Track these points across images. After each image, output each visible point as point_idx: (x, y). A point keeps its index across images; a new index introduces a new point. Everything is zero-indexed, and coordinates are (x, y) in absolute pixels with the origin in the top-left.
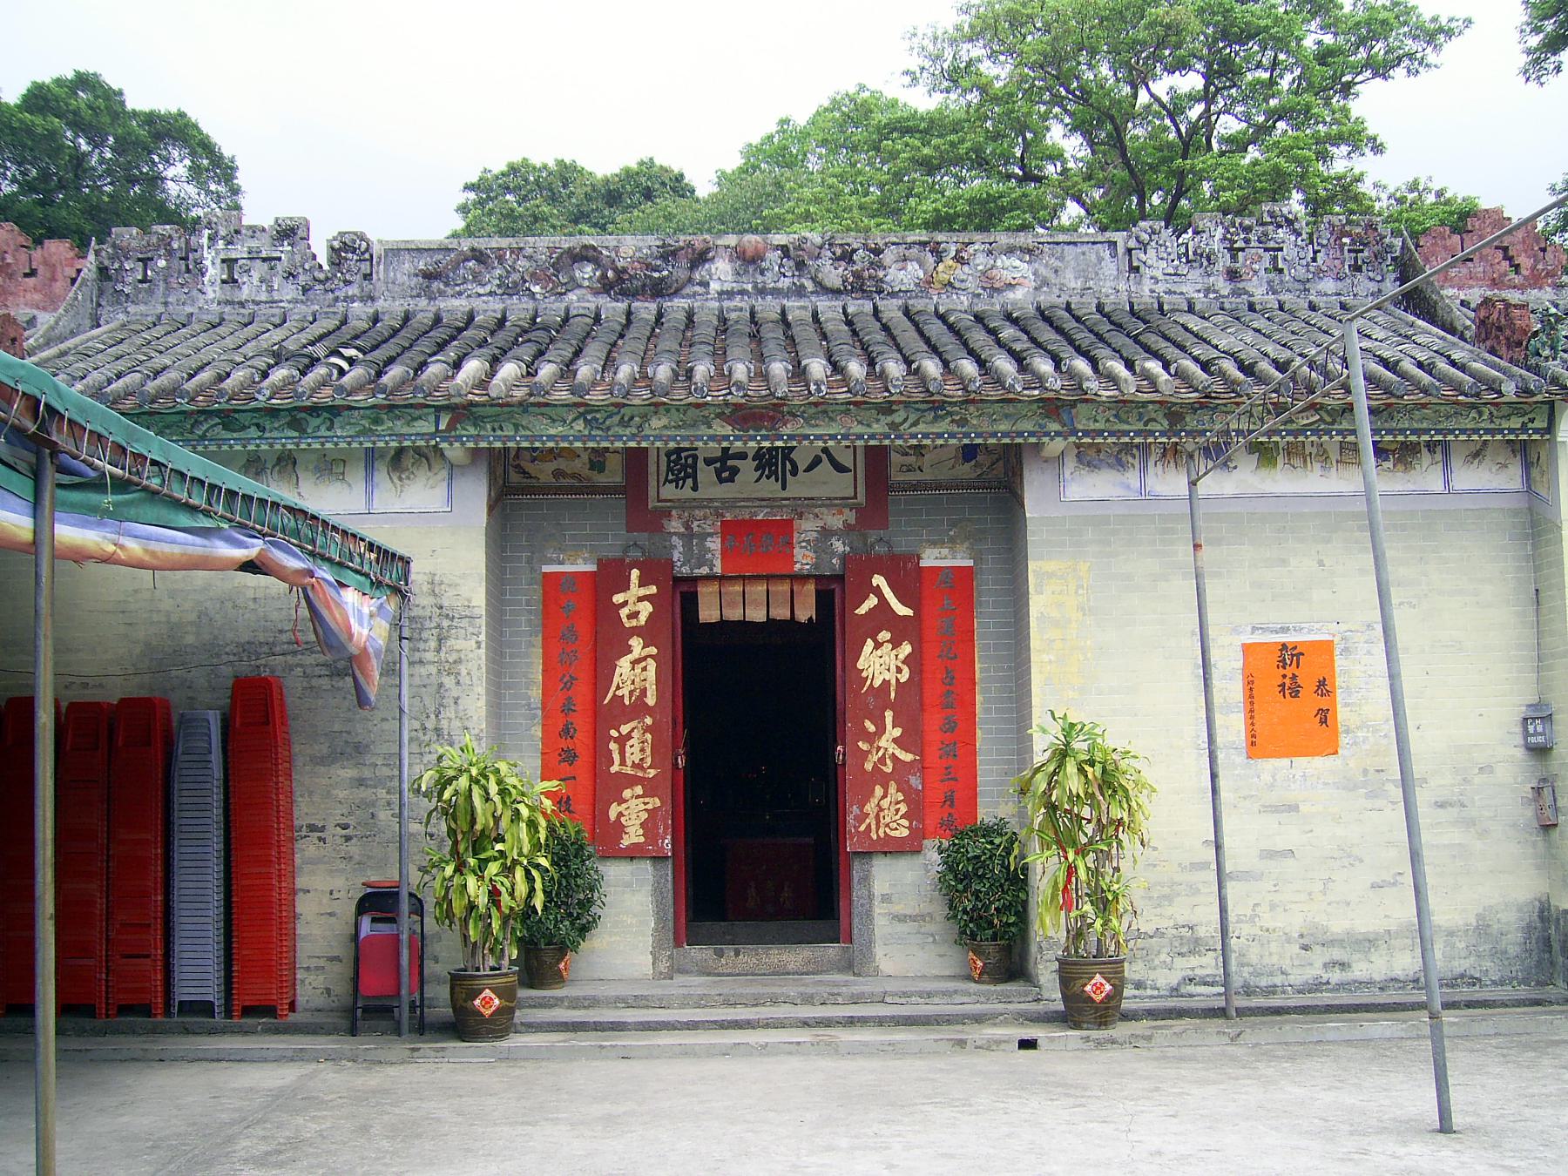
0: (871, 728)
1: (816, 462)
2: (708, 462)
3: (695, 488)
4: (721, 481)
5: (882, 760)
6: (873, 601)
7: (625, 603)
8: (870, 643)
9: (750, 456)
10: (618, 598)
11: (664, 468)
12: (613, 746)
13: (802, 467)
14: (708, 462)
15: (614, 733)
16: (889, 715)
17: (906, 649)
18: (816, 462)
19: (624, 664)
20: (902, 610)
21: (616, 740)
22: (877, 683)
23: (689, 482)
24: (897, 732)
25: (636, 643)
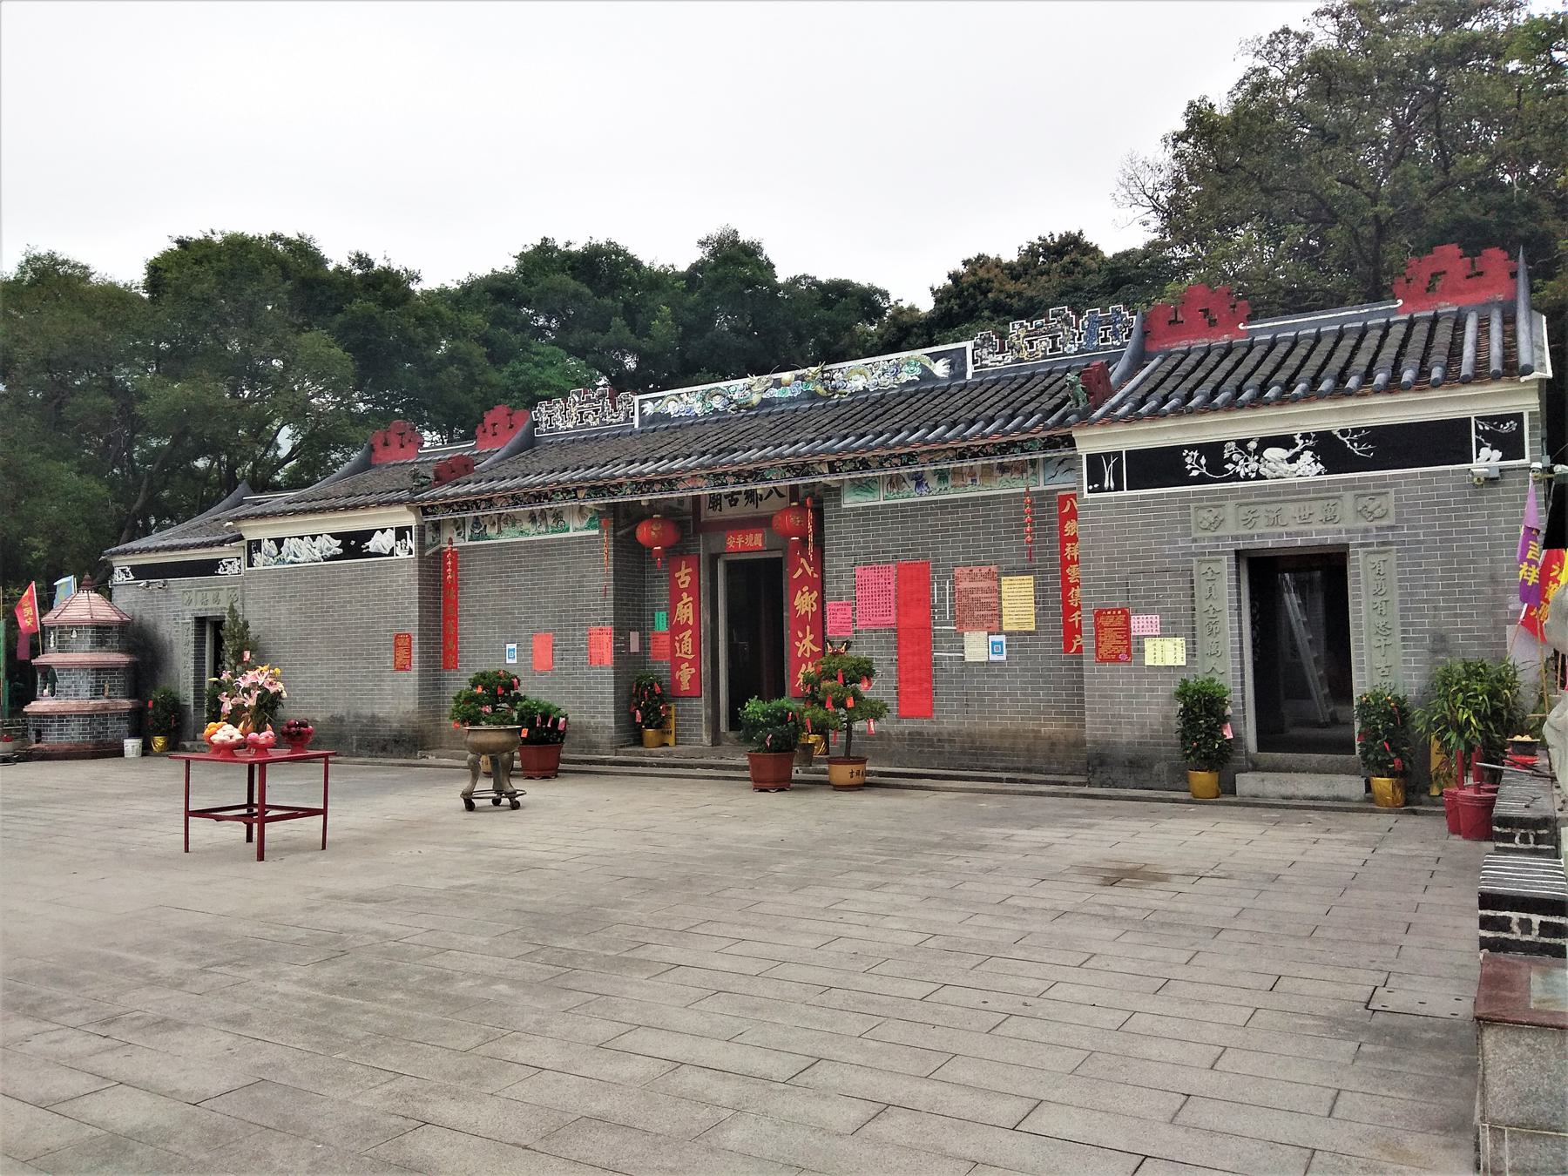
6: (800, 571)
17: (815, 594)
19: (680, 605)
25: (685, 595)
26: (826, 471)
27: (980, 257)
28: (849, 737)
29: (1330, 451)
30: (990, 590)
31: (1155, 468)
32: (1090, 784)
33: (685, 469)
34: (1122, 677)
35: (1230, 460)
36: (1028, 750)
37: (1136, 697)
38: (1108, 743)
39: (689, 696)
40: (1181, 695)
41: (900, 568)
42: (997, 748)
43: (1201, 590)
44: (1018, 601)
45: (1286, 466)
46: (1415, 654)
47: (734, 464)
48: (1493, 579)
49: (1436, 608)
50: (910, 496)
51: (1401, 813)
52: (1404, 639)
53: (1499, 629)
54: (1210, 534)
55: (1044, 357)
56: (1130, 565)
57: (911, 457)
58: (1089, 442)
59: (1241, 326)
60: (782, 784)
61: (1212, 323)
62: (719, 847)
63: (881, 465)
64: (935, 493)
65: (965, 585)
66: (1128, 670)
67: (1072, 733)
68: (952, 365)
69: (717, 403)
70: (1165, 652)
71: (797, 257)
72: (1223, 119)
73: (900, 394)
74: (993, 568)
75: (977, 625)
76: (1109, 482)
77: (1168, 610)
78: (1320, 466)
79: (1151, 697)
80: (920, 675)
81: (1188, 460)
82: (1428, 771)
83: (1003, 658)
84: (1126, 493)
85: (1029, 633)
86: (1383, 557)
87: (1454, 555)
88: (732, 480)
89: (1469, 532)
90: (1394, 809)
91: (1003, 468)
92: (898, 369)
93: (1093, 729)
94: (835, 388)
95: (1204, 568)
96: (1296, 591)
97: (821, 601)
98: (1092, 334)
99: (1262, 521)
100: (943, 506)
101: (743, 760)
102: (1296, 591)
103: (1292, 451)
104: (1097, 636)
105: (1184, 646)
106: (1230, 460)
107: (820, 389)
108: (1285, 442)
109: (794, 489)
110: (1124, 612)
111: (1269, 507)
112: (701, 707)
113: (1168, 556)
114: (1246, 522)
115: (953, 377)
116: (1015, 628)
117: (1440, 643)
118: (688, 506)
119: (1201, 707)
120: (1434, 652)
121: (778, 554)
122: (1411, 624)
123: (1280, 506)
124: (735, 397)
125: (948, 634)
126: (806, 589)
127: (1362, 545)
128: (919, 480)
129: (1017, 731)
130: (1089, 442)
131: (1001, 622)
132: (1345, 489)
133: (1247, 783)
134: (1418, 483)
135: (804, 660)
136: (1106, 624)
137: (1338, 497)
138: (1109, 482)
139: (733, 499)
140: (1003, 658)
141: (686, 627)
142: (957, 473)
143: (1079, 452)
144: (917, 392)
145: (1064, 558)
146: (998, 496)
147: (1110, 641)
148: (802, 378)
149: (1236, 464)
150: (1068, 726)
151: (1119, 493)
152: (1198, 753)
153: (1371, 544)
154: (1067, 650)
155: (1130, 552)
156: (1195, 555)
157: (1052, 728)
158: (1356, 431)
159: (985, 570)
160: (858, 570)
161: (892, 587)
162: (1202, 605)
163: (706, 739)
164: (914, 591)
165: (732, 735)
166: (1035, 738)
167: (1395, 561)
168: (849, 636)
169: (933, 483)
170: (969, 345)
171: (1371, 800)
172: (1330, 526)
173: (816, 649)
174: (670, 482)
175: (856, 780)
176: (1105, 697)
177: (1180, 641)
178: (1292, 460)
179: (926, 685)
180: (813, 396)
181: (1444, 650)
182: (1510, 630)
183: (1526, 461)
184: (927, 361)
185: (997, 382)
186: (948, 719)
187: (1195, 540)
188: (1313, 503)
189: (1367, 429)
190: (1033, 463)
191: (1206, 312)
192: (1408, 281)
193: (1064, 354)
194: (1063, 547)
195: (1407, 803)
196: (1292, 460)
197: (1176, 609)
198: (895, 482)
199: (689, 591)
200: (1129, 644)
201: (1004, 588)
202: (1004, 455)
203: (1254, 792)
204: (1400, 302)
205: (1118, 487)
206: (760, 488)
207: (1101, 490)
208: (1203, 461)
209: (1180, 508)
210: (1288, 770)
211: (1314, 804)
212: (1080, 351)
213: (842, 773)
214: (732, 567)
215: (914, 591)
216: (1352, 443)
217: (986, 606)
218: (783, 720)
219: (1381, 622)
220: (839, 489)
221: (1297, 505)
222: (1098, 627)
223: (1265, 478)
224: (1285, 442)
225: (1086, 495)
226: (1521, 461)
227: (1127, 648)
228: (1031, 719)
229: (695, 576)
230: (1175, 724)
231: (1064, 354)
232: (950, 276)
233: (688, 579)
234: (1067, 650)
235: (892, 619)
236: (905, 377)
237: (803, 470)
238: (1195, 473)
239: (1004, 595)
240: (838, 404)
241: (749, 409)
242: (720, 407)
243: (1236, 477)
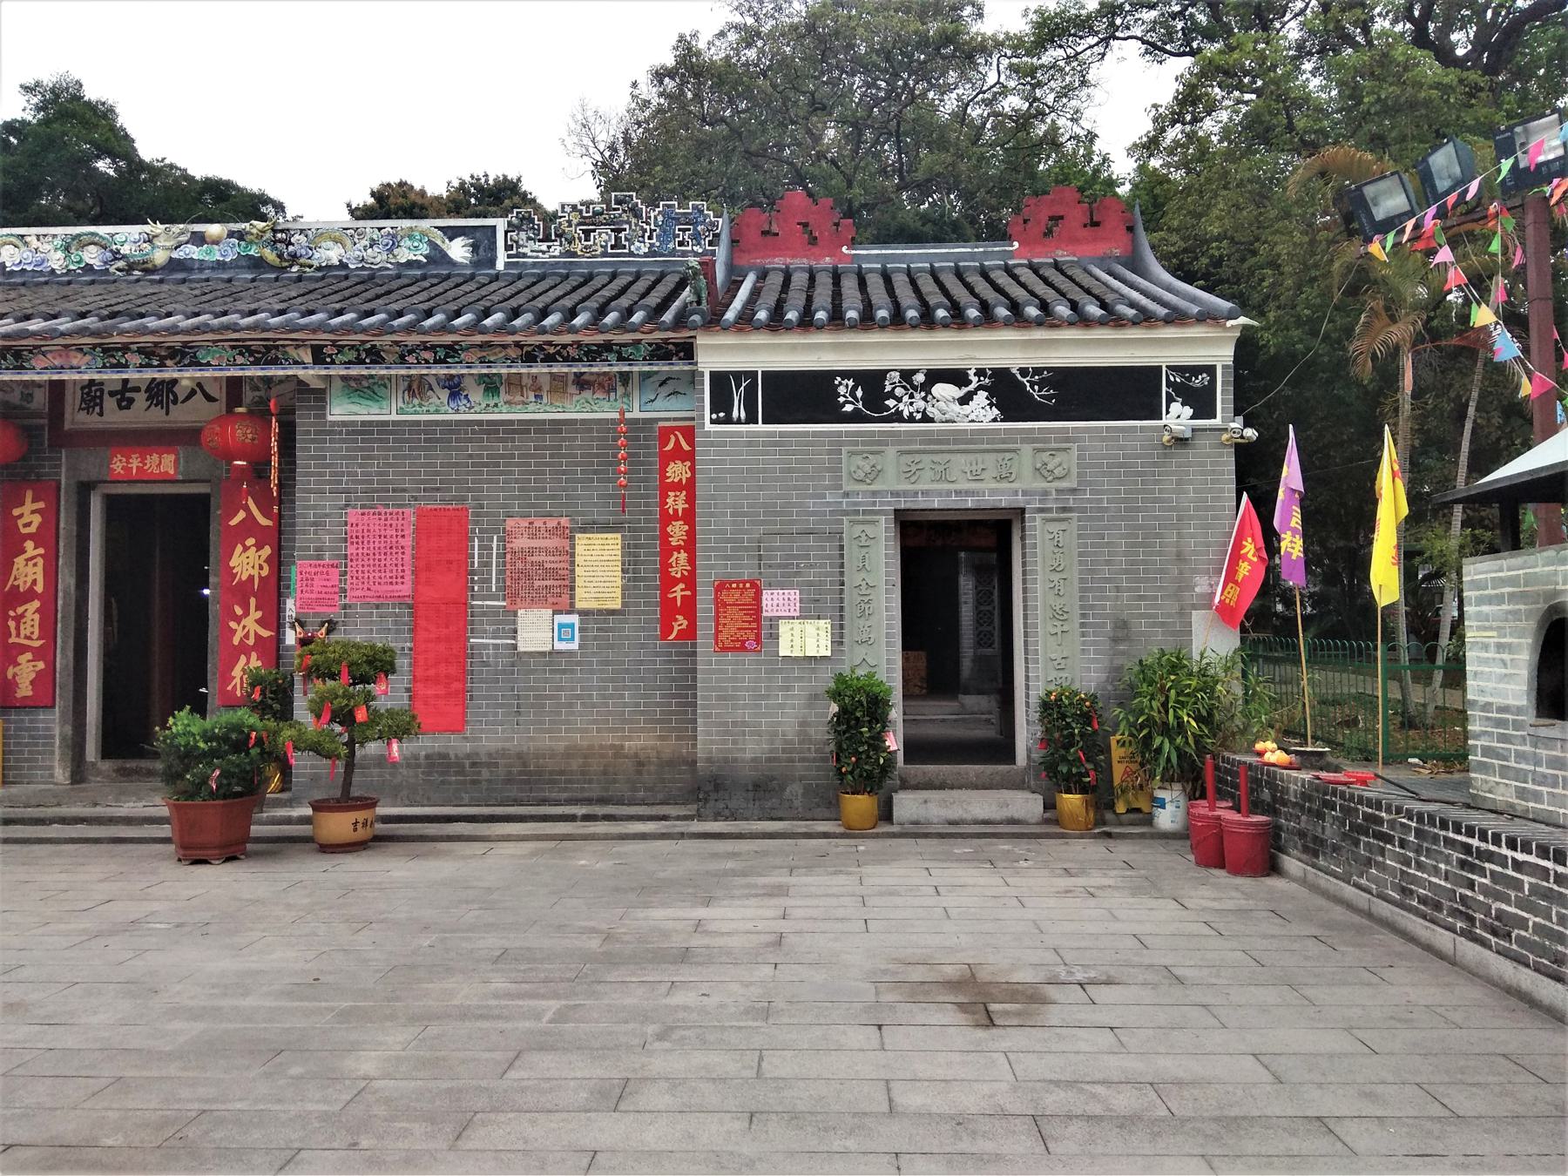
0: (239, 611)
1: (193, 393)
2: (112, 394)
3: (101, 414)
4: (121, 408)
5: (247, 636)
6: (241, 515)
7: (21, 516)
8: (239, 548)
9: (143, 388)
10: (16, 512)
11: (78, 402)
12: (12, 624)
13: (181, 398)
14: (112, 394)
15: (12, 613)
16: (253, 601)
17: (267, 551)
18: (193, 393)
19: (19, 561)
20: (263, 521)
21: (14, 618)
22: (244, 578)
23: (97, 409)
24: (259, 614)
25: (29, 545)
26: (308, 358)
27: (402, 184)
28: (350, 766)
29: (1007, 392)
30: (557, 551)
31: (798, 397)
32: (699, 817)
33: (53, 334)
34: (747, 671)
35: (891, 395)
36: (605, 773)
37: (767, 697)
38: (726, 760)
39: (29, 706)
40: (835, 695)
41: (421, 515)
42: (562, 773)
43: (852, 554)
44: (600, 568)
45: (957, 407)
46: (1094, 643)
47: (145, 331)
48: (1180, 557)
49: (1118, 589)
50: (438, 410)
51: (1095, 836)
52: (1083, 625)
53: (1184, 614)
54: (864, 487)
55: (605, 254)
56: (763, 523)
57: (451, 352)
58: (718, 354)
59: (844, 249)
60: (233, 850)
61: (813, 241)
62: (195, 1015)
63: (402, 360)
64: (478, 409)
65: (521, 543)
66: (758, 662)
67: (670, 747)
68: (475, 248)
69: (92, 256)
70: (804, 638)
71: (163, 136)
72: (713, 63)
73: (399, 277)
74: (564, 521)
75: (537, 600)
76: (738, 411)
77: (810, 584)
78: (995, 411)
79: (786, 697)
80: (450, 671)
81: (842, 390)
82: (1112, 787)
83: (575, 646)
84: (760, 427)
85: (613, 612)
86: (1063, 526)
87: (1141, 527)
88: (136, 359)
89: (1155, 500)
90: (1086, 833)
91: (582, 383)
92: (394, 241)
93: (708, 742)
94: (294, 257)
95: (858, 529)
96: (954, 567)
97: (278, 563)
98: (666, 235)
99: (928, 474)
100: (493, 429)
101: (165, 812)
102: (954, 567)
103: (965, 390)
104: (717, 618)
105: (828, 634)
106: (891, 395)
107: (270, 255)
108: (957, 377)
109: (234, 384)
110: (754, 585)
111: (937, 458)
112: (54, 723)
113: (814, 513)
114: (909, 475)
115: (476, 264)
116: (593, 605)
117: (1122, 630)
118: (40, 399)
119: (858, 711)
120: (1115, 640)
121: (202, 489)
122: (1092, 607)
123: (947, 457)
124: (125, 250)
125: (494, 611)
126: (250, 541)
127: (1041, 510)
128: (455, 388)
129: (591, 747)
130: (718, 354)
131: (572, 597)
132: (1023, 441)
133: (907, 805)
134: (1103, 439)
135: (243, 649)
136: (730, 600)
137: (1014, 451)
138: (738, 411)
139: (124, 395)
140: (575, 646)
141: (30, 595)
142: (514, 383)
143: (700, 367)
144: (424, 277)
145: (664, 512)
146: (574, 422)
147: (735, 622)
148: (241, 236)
149: (899, 400)
150: (661, 738)
151: (751, 427)
152: (853, 770)
153: (1049, 510)
154: (664, 636)
155: (764, 505)
156: (846, 513)
157: (640, 741)
158: (1037, 371)
159: (552, 523)
160: (353, 515)
161: (408, 542)
162: (853, 578)
163: (61, 774)
164: (443, 548)
165: (106, 766)
166: (616, 756)
167: (1075, 532)
168: (334, 613)
169: (477, 395)
170: (500, 224)
171: (1056, 822)
172: (1005, 485)
173: (265, 633)
174: (18, 355)
175: (362, 834)
176: (724, 698)
177: (825, 624)
178: (964, 400)
179: (456, 685)
180: (258, 264)
181: (1126, 639)
182: (1196, 616)
183: (1217, 422)
184: (438, 237)
185: (542, 278)
186: (489, 733)
187: (847, 495)
188: (987, 456)
189: (1049, 369)
190: (625, 378)
191: (805, 225)
192: (1025, 222)
193: (631, 254)
194: (664, 496)
195: (1096, 825)
196: (964, 400)
197: (821, 583)
198: (416, 388)
199: (37, 538)
200: (759, 628)
201: (579, 549)
202: (589, 364)
203: (915, 817)
204: (1016, 244)
205: (752, 419)
206: (186, 377)
207: (728, 420)
208: (859, 393)
209: (830, 452)
210: (942, 786)
211: (987, 831)
212: (652, 253)
213: (339, 825)
214: (111, 502)
215: (443, 548)
216: (1032, 384)
217: (553, 573)
218: (240, 746)
219: (1058, 603)
220: (323, 391)
221: (971, 457)
222: (720, 605)
223: (932, 420)
224: (957, 377)
225: (709, 427)
226: (1212, 421)
227: (755, 632)
228: (611, 730)
229: (50, 517)
230: (821, 732)
231: (631, 254)
232: (373, 194)
233: (37, 519)
234: (664, 636)
235: (406, 589)
236: (404, 255)
237: (267, 353)
238: (849, 408)
239: (578, 559)
240: (299, 279)
241: (147, 271)
242: (97, 264)
243: (898, 417)
